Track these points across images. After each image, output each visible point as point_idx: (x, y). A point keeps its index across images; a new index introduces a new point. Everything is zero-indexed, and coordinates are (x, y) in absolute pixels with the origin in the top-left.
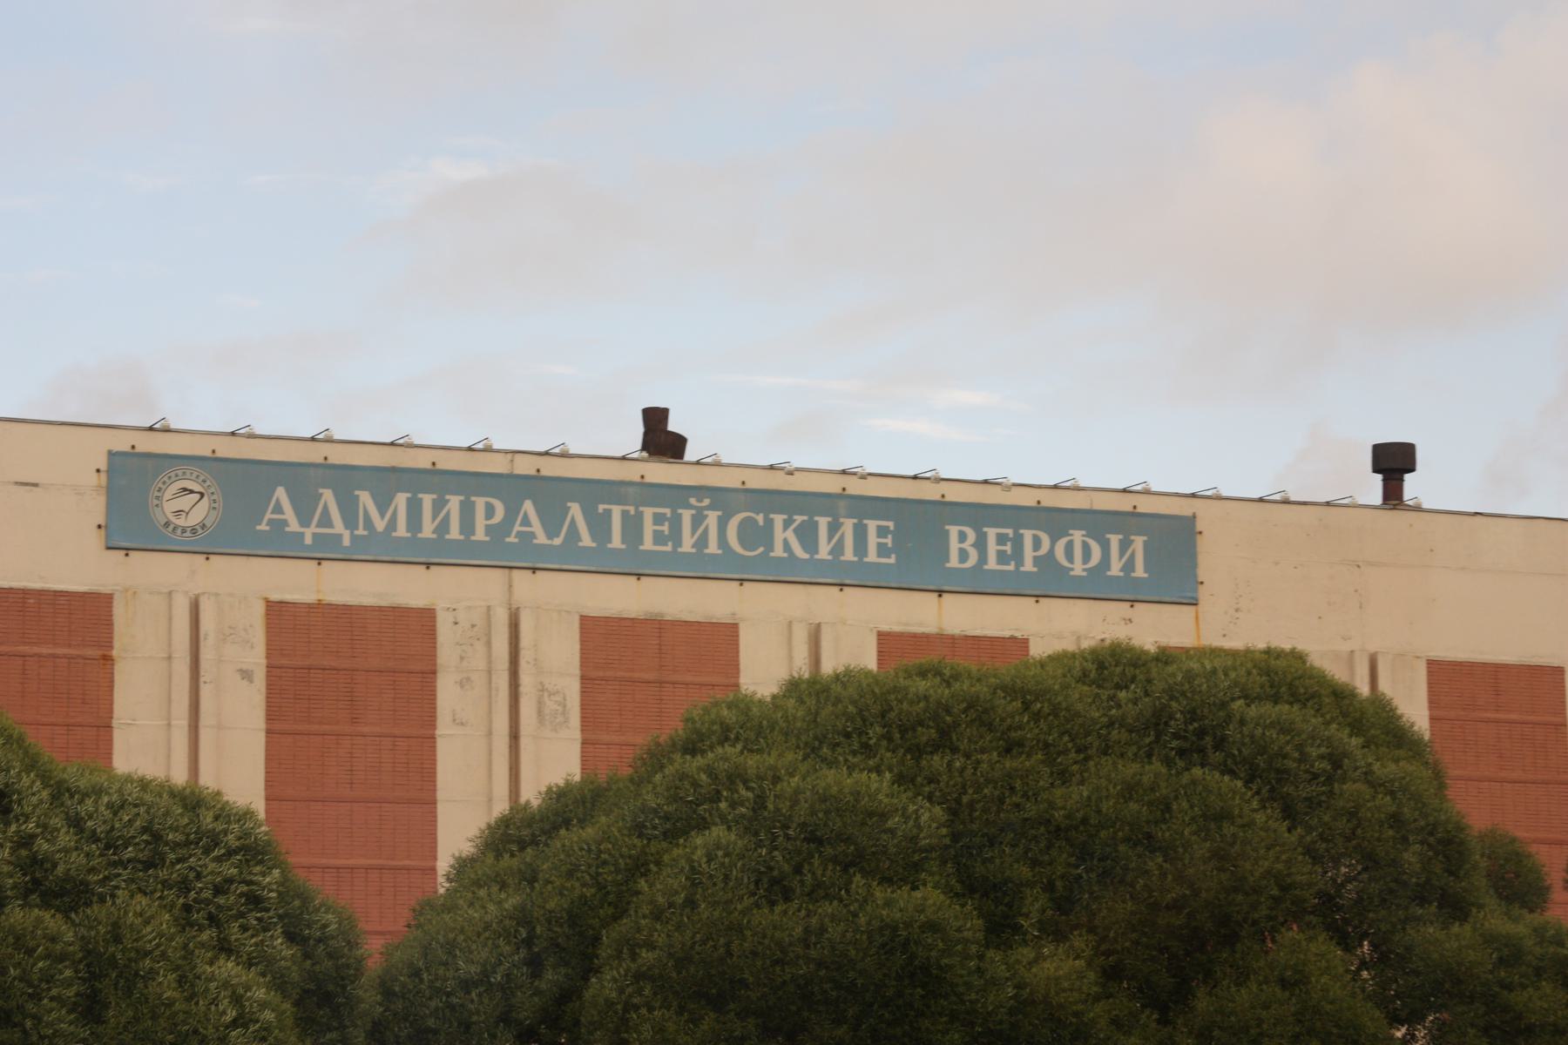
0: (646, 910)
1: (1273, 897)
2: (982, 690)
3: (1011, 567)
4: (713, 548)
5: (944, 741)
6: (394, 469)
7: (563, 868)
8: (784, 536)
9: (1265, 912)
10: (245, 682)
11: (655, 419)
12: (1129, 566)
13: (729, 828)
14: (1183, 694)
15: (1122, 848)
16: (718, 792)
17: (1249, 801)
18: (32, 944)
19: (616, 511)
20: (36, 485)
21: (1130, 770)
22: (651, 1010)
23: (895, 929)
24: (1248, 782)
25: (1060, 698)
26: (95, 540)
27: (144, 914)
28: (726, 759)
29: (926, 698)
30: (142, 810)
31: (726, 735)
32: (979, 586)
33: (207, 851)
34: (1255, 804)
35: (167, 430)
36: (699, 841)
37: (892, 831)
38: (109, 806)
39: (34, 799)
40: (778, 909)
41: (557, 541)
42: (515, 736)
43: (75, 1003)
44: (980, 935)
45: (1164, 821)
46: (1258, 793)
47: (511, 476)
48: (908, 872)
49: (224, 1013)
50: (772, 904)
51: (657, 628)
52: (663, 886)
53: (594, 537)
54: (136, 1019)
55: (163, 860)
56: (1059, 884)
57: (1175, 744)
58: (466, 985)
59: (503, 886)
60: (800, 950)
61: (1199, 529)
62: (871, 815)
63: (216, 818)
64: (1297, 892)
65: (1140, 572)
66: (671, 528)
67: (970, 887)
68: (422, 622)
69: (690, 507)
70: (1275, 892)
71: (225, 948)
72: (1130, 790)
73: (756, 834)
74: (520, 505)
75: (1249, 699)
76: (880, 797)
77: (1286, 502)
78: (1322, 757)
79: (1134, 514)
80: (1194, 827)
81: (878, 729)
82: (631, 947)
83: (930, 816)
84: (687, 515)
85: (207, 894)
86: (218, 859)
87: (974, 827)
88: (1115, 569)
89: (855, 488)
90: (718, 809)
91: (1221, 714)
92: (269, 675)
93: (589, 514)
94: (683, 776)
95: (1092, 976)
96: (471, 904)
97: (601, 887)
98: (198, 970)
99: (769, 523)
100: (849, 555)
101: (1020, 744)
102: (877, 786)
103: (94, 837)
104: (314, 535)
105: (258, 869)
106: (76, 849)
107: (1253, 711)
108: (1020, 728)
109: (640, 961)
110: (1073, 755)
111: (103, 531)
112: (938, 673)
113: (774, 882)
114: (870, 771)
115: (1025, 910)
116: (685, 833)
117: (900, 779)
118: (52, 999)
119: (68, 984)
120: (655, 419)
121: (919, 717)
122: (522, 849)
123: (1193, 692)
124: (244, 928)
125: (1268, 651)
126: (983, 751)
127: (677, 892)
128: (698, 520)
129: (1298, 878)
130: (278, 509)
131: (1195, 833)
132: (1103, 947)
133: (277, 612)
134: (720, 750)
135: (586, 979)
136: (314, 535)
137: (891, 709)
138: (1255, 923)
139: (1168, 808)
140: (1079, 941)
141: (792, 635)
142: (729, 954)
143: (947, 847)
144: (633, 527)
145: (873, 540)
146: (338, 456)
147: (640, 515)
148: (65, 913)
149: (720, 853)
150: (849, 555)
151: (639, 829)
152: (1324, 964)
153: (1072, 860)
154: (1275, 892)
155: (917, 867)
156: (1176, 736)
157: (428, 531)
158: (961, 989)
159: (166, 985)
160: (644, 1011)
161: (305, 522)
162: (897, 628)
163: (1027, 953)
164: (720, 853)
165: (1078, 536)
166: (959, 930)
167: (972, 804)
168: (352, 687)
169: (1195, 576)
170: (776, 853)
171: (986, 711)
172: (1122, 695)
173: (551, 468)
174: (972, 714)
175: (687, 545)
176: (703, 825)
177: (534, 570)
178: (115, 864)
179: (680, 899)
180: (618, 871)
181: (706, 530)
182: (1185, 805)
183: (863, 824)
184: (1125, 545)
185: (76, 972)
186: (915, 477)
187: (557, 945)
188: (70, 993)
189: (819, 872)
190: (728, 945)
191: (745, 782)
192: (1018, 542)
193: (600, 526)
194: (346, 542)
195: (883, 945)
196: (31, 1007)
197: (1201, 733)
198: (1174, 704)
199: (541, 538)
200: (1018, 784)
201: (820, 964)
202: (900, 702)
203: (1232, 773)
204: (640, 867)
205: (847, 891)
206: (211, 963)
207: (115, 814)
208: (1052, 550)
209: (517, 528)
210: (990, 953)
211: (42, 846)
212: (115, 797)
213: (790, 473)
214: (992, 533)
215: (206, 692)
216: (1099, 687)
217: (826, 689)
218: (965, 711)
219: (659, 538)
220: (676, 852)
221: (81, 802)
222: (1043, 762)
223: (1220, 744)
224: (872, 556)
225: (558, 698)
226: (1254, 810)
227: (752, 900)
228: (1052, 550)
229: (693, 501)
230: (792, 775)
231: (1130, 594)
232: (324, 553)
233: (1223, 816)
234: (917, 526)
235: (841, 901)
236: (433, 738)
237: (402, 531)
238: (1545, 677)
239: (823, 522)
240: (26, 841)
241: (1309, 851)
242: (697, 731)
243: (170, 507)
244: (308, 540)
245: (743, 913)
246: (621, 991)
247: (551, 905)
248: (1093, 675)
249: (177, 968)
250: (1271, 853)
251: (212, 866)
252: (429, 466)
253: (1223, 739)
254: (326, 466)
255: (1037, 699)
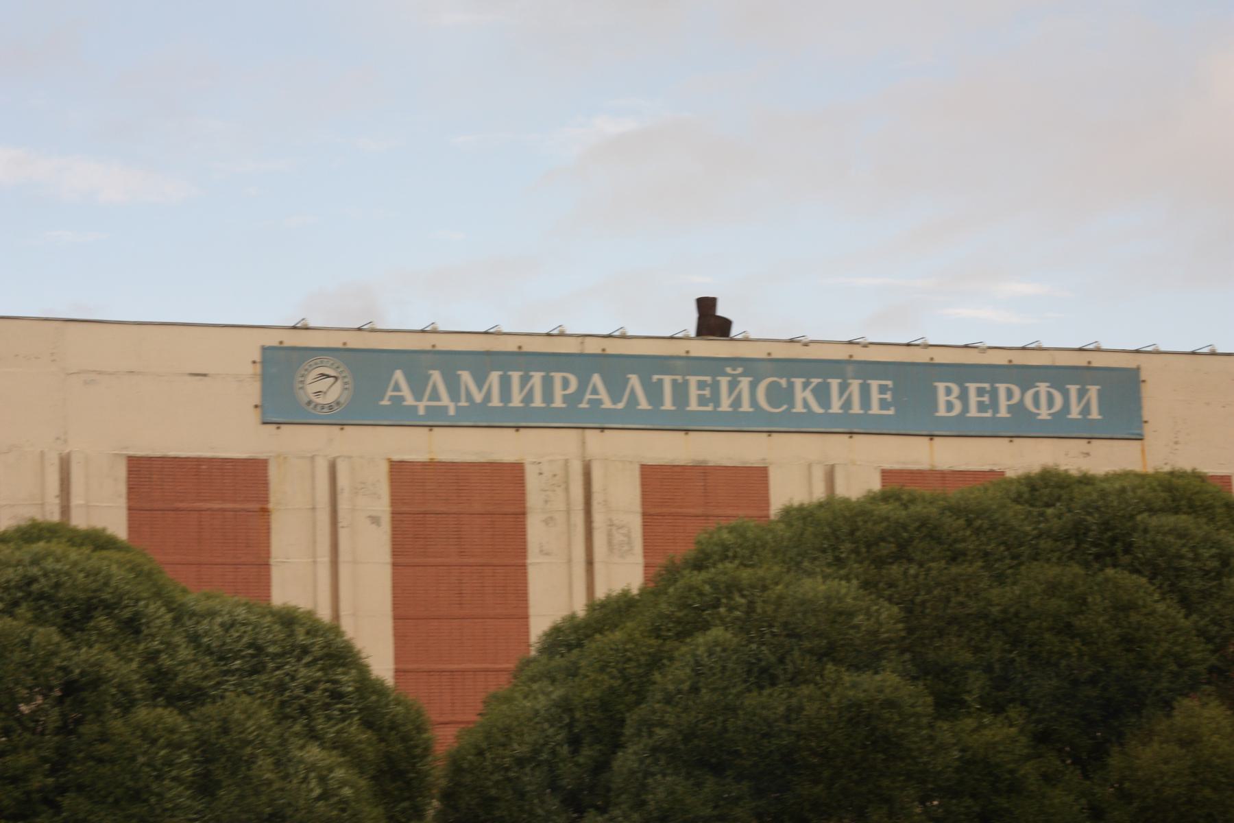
0: (659, 696)
1: (1171, 672)
2: (934, 510)
3: (988, 414)
4: (746, 407)
5: (902, 553)
6: (488, 353)
7: (597, 665)
8: (803, 396)
9: (1166, 685)
10: (374, 526)
11: (706, 306)
12: (1086, 410)
13: (726, 629)
14: (1097, 509)
15: (1047, 636)
16: (718, 600)
17: (1151, 595)
18: (155, 735)
19: (667, 380)
20: (205, 375)
21: (1052, 571)
22: (664, 775)
23: (860, 706)
24: (1151, 579)
25: (997, 516)
26: (253, 417)
27: (248, 711)
28: (725, 574)
29: (887, 519)
30: (250, 628)
31: (725, 553)
32: (963, 430)
33: (299, 659)
34: (1156, 596)
35: (307, 328)
36: (701, 640)
37: (857, 627)
38: (222, 625)
39: (158, 622)
40: (766, 692)
41: (621, 406)
42: (590, 563)
43: (193, 782)
44: (930, 710)
45: (1082, 612)
46: (1160, 587)
47: (581, 355)
48: (868, 657)
49: (312, 790)
50: (761, 688)
51: (702, 472)
52: (675, 675)
53: (650, 402)
54: (241, 797)
55: (264, 667)
56: (997, 666)
57: (1094, 550)
58: (520, 762)
59: (553, 681)
60: (782, 724)
61: (1143, 378)
62: (841, 614)
63: (308, 633)
64: (1193, 668)
65: (1095, 414)
66: (712, 393)
67: (928, 671)
68: (514, 474)
69: (727, 375)
70: (1174, 668)
71: (313, 735)
72: (1052, 589)
73: (748, 633)
74: (594, 377)
75: (1152, 510)
76: (849, 600)
77: (1213, 354)
78: (1212, 556)
79: (1089, 368)
80: (1106, 617)
81: (848, 545)
82: (647, 725)
83: (888, 613)
84: (724, 382)
85: (298, 692)
86: (308, 665)
87: (926, 621)
88: (1075, 413)
89: (860, 355)
90: (718, 613)
91: (1129, 524)
92: (393, 520)
93: (646, 384)
94: (691, 588)
95: (1023, 740)
96: (526, 697)
97: (626, 679)
98: (290, 755)
99: (791, 386)
100: (856, 409)
101: (964, 553)
102: (847, 591)
103: (209, 651)
104: (427, 407)
105: (340, 670)
106: (194, 661)
107: (1154, 521)
108: (964, 540)
109: (656, 737)
110: (1008, 561)
111: (259, 410)
112: (898, 499)
113: (764, 671)
114: (841, 579)
115: (968, 688)
116: (690, 634)
117: (866, 585)
118: (174, 779)
119: (185, 766)
120: (706, 306)
121: (883, 537)
122: (569, 650)
123: (1107, 506)
124: (329, 718)
125: (1172, 473)
126: (933, 560)
127: (683, 682)
128: (733, 385)
129: (1194, 656)
130: (397, 388)
131: (1106, 621)
132: (1034, 717)
133: (399, 470)
134: (720, 566)
135: (614, 753)
136: (427, 407)
137: (858, 529)
138: (1158, 693)
139: (1085, 602)
140: (1013, 712)
141: (805, 471)
142: (725, 730)
143: (904, 638)
144: (680, 392)
145: (875, 396)
146: (444, 344)
147: (686, 383)
148: (183, 711)
149: (718, 649)
150: (856, 409)
151: (656, 632)
152: (1213, 726)
153: (1007, 647)
154: (1174, 668)
155: (878, 656)
156: (1094, 544)
157: (516, 401)
158: (916, 754)
159: (264, 768)
160: (659, 777)
161: (418, 397)
162: (897, 467)
163: (970, 723)
164: (718, 649)
165: (1043, 387)
166: (912, 706)
167: (923, 603)
168: (456, 529)
169: (1140, 416)
170: (763, 648)
171: (935, 528)
172: (1050, 511)
173: (614, 348)
174: (924, 530)
175: (725, 405)
176: (706, 626)
177: (603, 429)
178: (226, 673)
179: (685, 687)
180: (639, 666)
181: (850, 396)
182: (1098, 598)
183: (834, 622)
184: (1082, 393)
185: (194, 756)
186: (908, 345)
187: (592, 727)
188: (188, 773)
189: (799, 662)
190: (725, 721)
191: (740, 590)
192: (994, 394)
193: (655, 393)
194: (452, 412)
195: (850, 720)
196: (155, 787)
197: (1114, 540)
198: (1088, 518)
199: (607, 404)
200: (962, 586)
201: (799, 735)
202: (866, 522)
203: (1138, 572)
204: (656, 662)
205: (822, 676)
206: (302, 748)
207: (227, 631)
208: (1022, 400)
209: (588, 396)
210: (939, 723)
211: (165, 661)
212: (226, 618)
213: (806, 345)
214: (972, 387)
215: (343, 535)
216: (1032, 505)
217: (811, 514)
218: (918, 529)
219: (702, 401)
220: (684, 649)
221: (198, 623)
222: (982, 567)
223: (1128, 549)
224: (875, 409)
225: (624, 531)
226: (1157, 601)
227: (744, 686)
228: (1022, 400)
229: (729, 370)
230: (777, 584)
231: (1088, 433)
232: (434, 421)
233: (1129, 607)
234: (911, 383)
235: (816, 684)
236: (524, 566)
237: (496, 402)
238: (1226, 479)
239: (835, 383)
240: (152, 656)
241: (1202, 633)
242: (702, 551)
243: (311, 389)
244: (421, 412)
245: (738, 695)
246: (641, 761)
247: (587, 695)
248: (1026, 496)
249: (274, 753)
250: (1171, 636)
251: (303, 672)
252: (515, 349)
253: (1131, 544)
254: (434, 352)
255: (978, 517)
